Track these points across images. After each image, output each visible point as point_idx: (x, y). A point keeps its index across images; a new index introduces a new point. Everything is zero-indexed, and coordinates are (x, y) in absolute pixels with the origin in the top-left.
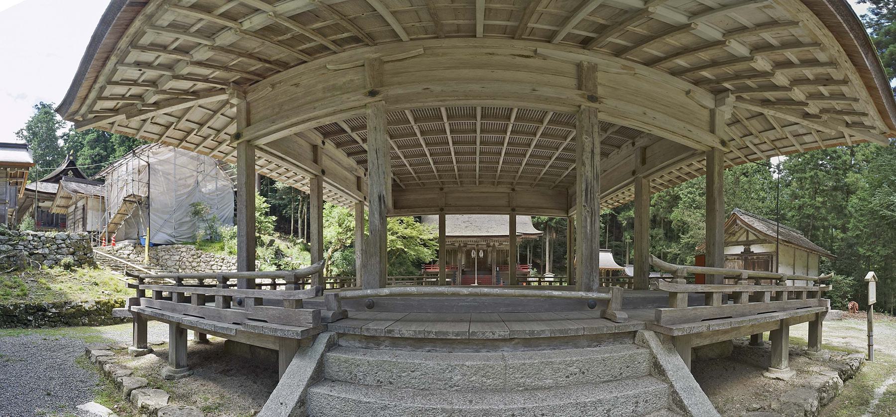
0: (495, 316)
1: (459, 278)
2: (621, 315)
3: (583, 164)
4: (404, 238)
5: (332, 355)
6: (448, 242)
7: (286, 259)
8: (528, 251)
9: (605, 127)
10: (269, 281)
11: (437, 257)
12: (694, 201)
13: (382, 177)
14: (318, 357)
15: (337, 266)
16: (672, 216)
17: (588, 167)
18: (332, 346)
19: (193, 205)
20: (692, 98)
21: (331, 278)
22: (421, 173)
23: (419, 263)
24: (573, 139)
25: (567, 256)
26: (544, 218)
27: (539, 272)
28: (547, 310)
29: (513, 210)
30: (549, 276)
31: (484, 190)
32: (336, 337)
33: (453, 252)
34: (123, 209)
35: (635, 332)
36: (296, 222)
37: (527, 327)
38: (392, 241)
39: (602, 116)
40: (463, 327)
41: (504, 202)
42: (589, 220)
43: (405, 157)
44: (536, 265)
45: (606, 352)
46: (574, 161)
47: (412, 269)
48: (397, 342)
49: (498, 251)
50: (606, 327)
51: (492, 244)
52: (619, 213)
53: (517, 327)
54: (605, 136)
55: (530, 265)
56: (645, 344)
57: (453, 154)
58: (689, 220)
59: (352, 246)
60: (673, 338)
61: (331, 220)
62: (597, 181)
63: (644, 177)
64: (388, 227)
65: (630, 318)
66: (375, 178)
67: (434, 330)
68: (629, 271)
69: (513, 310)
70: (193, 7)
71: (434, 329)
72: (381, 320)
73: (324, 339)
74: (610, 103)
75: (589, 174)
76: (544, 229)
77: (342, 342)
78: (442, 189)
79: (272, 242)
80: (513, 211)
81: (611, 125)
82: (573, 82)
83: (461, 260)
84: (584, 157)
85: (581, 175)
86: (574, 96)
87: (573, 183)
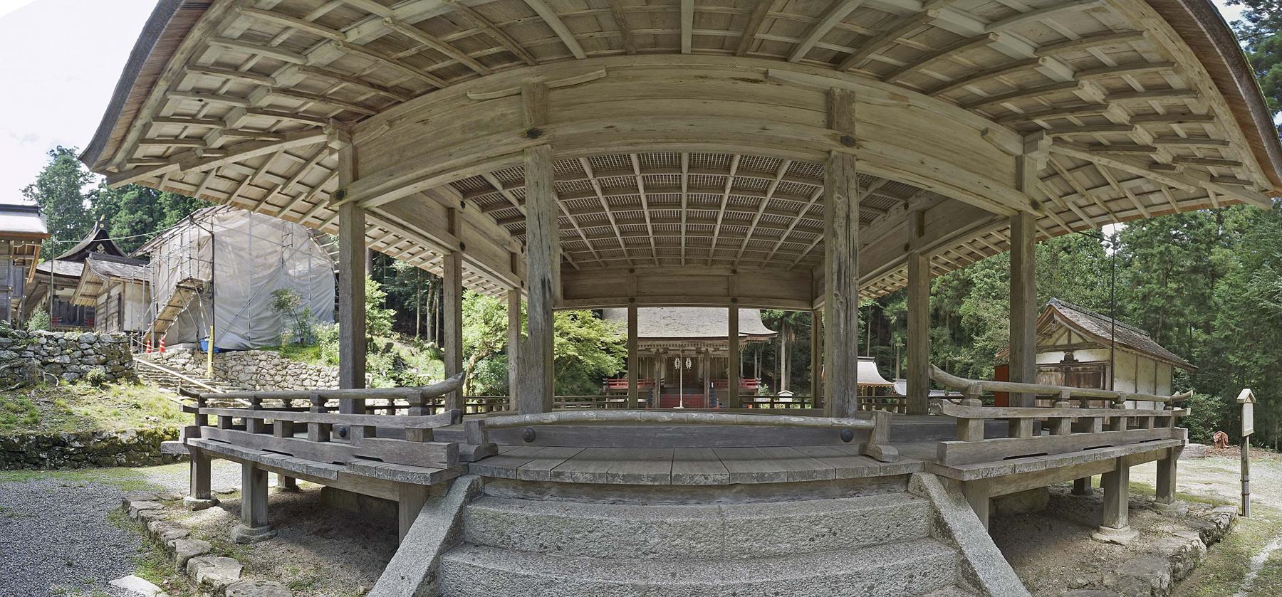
0: (709, 453)
1: (657, 398)
2: (889, 451)
3: (835, 235)
4: (579, 340)
5: (475, 508)
6: (641, 346)
7: (409, 371)
8: (756, 360)
9: (865, 181)
10: (385, 402)
11: (625, 368)
12: (993, 287)
13: (546, 253)
14: (455, 511)
15: (482, 381)
16: (961, 310)
17: (841, 240)
18: (474, 495)
19: (276, 293)
20: (991, 141)
21: (473, 398)
22: (603, 247)
23: (599, 377)
24: (820, 200)
25: (812, 366)
26: (779, 312)
27: (771, 389)
28: (782, 445)
29: (734, 300)
30: (786, 396)
31: (692, 272)
32: (481, 482)
33: (649, 361)
34: (176, 299)
35: (909, 475)
36: (424, 318)
37: (755, 469)
38: (561, 345)
39: (861, 167)
40: (663, 469)
41: (721, 289)
42: (842, 315)
43: (580, 225)
44: (766, 380)
45: (867, 504)
46: (821, 231)
47: (590, 385)
48: (568, 489)
49: (713, 360)
50: (867, 468)
51: (703, 349)
52: (885, 305)
53: (739, 468)
54: (865, 195)
55: (758, 380)
56: (923, 493)
57: (648, 220)
58: (986, 315)
59: (503, 352)
60: (963, 485)
61: (474, 315)
62: (855, 260)
63: (922, 254)
64: (556, 325)
65: (902, 455)
66: (537, 255)
67: (621, 473)
68: (901, 388)
69: (734, 444)
70: (277, 10)
71: (620, 471)
72: (545, 458)
73: (463, 485)
74: (873, 147)
75: (843, 250)
76: (779, 328)
77: (490, 490)
78: (632, 271)
79: (389, 346)
80: (734, 303)
81: (875, 179)
82: (820, 118)
83: (659, 373)
84: (836, 225)
85: (832, 251)
86: (822, 137)
87: (820, 262)
